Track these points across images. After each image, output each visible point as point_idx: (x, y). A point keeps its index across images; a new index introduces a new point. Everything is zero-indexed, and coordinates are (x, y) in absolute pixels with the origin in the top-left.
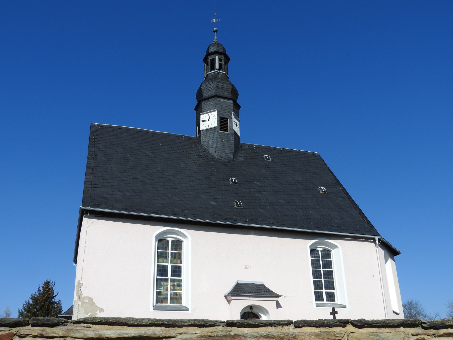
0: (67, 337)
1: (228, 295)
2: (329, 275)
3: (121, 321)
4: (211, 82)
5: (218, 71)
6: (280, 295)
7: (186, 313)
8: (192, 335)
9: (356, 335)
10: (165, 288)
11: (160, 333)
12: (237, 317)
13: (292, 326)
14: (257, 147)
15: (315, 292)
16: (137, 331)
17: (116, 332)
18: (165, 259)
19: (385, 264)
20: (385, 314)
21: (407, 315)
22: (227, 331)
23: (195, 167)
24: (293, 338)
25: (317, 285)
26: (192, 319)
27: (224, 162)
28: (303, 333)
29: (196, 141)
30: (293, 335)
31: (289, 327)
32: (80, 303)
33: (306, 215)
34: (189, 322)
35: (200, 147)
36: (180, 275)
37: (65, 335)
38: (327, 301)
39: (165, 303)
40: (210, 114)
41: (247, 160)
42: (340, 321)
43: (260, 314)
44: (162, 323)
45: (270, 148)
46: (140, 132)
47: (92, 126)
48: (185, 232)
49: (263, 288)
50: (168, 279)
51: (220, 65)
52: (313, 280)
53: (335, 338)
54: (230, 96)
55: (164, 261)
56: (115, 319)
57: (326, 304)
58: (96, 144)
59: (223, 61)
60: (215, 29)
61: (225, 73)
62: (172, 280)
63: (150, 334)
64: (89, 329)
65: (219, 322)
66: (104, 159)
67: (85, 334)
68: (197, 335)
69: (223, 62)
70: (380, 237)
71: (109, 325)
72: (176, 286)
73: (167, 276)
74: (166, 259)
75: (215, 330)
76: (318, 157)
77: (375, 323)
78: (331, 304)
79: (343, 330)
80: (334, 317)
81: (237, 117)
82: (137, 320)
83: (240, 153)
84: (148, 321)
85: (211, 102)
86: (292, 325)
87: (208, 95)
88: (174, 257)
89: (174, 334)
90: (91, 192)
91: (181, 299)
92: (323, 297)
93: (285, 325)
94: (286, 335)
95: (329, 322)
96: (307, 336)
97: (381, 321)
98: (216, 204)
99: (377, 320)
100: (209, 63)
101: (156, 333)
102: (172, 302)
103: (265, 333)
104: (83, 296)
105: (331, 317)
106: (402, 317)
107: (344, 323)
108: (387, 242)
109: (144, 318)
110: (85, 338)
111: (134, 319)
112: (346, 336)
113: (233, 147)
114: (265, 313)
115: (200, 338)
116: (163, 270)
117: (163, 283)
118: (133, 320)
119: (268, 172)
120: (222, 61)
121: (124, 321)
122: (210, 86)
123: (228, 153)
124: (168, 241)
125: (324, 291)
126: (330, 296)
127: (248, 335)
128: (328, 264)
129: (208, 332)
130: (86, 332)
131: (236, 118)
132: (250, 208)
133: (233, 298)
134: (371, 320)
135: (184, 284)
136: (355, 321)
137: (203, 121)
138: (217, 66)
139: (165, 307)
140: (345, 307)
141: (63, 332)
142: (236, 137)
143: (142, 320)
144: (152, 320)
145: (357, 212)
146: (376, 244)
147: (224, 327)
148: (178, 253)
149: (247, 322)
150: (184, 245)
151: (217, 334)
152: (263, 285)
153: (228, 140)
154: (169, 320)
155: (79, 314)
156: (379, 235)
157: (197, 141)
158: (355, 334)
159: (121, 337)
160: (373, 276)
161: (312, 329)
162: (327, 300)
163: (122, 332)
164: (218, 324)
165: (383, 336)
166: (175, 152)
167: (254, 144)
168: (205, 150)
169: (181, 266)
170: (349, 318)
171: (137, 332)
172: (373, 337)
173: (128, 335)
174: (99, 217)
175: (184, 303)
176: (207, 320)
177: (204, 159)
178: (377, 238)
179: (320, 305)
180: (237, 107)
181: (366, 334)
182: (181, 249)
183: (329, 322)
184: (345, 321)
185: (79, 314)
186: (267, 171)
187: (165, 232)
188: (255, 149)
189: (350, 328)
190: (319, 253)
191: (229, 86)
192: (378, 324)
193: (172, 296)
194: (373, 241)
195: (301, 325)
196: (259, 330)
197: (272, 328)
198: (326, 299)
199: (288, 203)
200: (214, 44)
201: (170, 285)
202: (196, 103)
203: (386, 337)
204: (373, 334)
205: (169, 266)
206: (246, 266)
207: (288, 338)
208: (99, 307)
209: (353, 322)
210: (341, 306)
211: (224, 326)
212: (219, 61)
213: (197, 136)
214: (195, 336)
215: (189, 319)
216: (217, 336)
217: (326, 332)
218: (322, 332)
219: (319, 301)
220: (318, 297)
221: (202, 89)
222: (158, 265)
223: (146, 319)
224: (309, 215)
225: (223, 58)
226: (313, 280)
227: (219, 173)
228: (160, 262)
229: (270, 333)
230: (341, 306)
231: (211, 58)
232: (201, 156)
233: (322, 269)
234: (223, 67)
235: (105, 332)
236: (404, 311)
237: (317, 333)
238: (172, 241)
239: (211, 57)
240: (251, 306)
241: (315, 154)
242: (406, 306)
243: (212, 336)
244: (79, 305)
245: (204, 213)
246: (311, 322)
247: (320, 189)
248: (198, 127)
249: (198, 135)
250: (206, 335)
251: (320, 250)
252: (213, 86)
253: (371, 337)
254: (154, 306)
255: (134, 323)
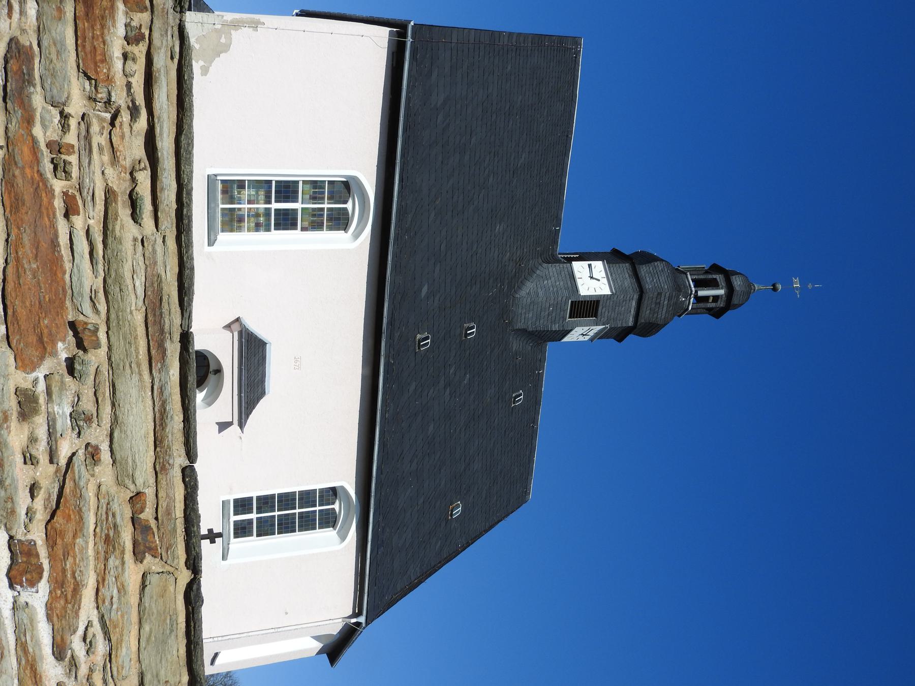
0: (152, 12)
1: (241, 324)
2: (286, 526)
3: (186, 120)
4: (670, 282)
5: (692, 296)
6: (245, 429)
7: (204, 242)
8: (162, 265)
9: (172, 588)
10: (252, 198)
11: (164, 200)
12: (199, 344)
13: (186, 462)
14: (540, 376)
15: (251, 499)
16: (168, 154)
17: (163, 111)
18: (310, 196)
19: (312, 637)
20: (213, 638)
21: (212, 679)
22: (173, 333)
23: (496, 252)
24: (161, 464)
25: (265, 502)
26: (193, 263)
27: (508, 311)
28: (173, 484)
29: (550, 254)
30: (167, 465)
31: (182, 456)
32: (218, 26)
33: (404, 478)
34: (188, 257)
35: (536, 262)
36: (278, 227)
37: (155, 9)
38: (234, 521)
39: (222, 199)
40: (605, 281)
41: (512, 358)
42: (198, 556)
43: (206, 390)
44: (184, 204)
45: (537, 403)
46: (567, 140)
47: (576, 41)
48: (365, 236)
49: (256, 394)
50: (269, 202)
51: (705, 299)
52: (275, 494)
53: (165, 548)
54: (642, 320)
55: (306, 194)
56: (190, 109)
57: (229, 519)
58: (540, 50)
59: (713, 305)
60: (779, 287)
61: (690, 309)
62: (268, 211)
63: (162, 180)
64: (170, 56)
65: (190, 317)
66: (509, 68)
67: (160, 48)
68: (163, 274)
69: (711, 305)
70: (364, 625)
71: (178, 96)
72: (257, 220)
73: (276, 201)
74: (310, 199)
75: (173, 310)
76: (522, 499)
77: (197, 626)
78: (229, 530)
79: (180, 562)
80: (204, 537)
81: (601, 336)
82: (190, 153)
83: (526, 344)
84: (187, 175)
85: (628, 282)
86: (186, 463)
87: (643, 275)
88: (314, 215)
89: (163, 227)
90: (442, 42)
91: (232, 231)
92: (242, 514)
93: (188, 449)
94: (168, 450)
95: (194, 536)
96: (166, 492)
97: (199, 638)
98: (423, 296)
99: (202, 628)
100: (710, 276)
101: (164, 192)
102: (226, 212)
103: (170, 410)
104: (233, 32)
105: (204, 531)
106: (209, 670)
107: (194, 564)
108: (356, 639)
109: (192, 168)
110: (151, 49)
111: (191, 146)
112: (168, 568)
113: (538, 329)
114: (208, 400)
115: (157, 281)
116: (288, 192)
117: (262, 193)
118: (189, 144)
119: (489, 399)
120: (713, 301)
121: (185, 127)
122: (662, 279)
123: (526, 319)
124: (345, 202)
125: (253, 516)
126: (244, 528)
127: (165, 374)
128: (307, 523)
129: (169, 295)
130: (163, 50)
131: (597, 334)
132: (415, 366)
133: (236, 334)
134: (201, 617)
135: (262, 235)
136: (198, 587)
137: (590, 266)
138: (702, 293)
139: (215, 199)
140: (224, 557)
141: (163, 5)
142: (559, 334)
143: (190, 163)
144: (190, 183)
145: (413, 579)
146: (350, 617)
147: (180, 328)
148: (323, 223)
149: (191, 374)
150: (341, 233)
151: (166, 313)
152: (263, 394)
153: (553, 318)
154: (190, 218)
155: (197, 25)
156: (367, 623)
157: (550, 256)
158: (173, 586)
159: (154, 122)
160: (286, 613)
161: (180, 502)
162: (236, 523)
163: (165, 123)
164: (186, 315)
165: (171, 641)
166: (526, 212)
167: (546, 370)
168: (532, 271)
169: (296, 229)
170: (203, 574)
171: (165, 153)
172: (168, 621)
173: (158, 135)
174: (393, 61)
175: (224, 238)
176: (193, 294)
177: (514, 270)
178: (362, 619)
179: (226, 508)
180: (620, 335)
181: (174, 609)
182: (330, 228)
183: (194, 536)
184: (197, 567)
185: (197, 25)
186: (491, 398)
187: (363, 195)
188: (534, 373)
189: (185, 576)
190: (329, 504)
191: (662, 317)
192: (194, 631)
193: (236, 213)
194: (357, 612)
195: (187, 480)
196: (176, 398)
197: (180, 423)
198: (239, 521)
199: (428, 443)
200: (749, 286)
201: (258, 209)
202: (627, 252)
203: (168, 648)
204: (173, 622)
205: (297, 206)
206: (299, 359)
207: (162, 455)
208: (212, 65)
209: (196, 582)
210: (226, 551)
211: (181, 328)
212: (713, 296)
213: (560, 256)
214: (161, 270)
215: (193, 258)
216: (161, 314)
217: (174, 530)
218: (176, 522)
219: (235, 507)
220: (242, 505)
221: (656, 264)
222: (297, 182)
223: (192, 172)
224: (404, 483)
225: (721, 304)
226: (275, 494)
227: (485, 302)
228: (305, 185)
229: (169, 419)
230: (226, 551)
231: (719, 280)
232: (519, 263)
233: (297, 511)
234: (702, 305)
235: (164, 90)
236: (218, 674)
237: (174, 511)
238: (346, 209)
239: (721, 279)
240: (222, 371)
241: (526, 493)
242: (228, 678)
243: (161, 304)
244: (214, 24)
245: (405, 273)
246: (194, 501)
247: (456, 505)
248: (577, 256)
249: (563, 256)
250: (163, 292)
251: (336, 506)
252: (662, 285)
253: (169, 617)
254: (216, 176)
255: (183, 146)
